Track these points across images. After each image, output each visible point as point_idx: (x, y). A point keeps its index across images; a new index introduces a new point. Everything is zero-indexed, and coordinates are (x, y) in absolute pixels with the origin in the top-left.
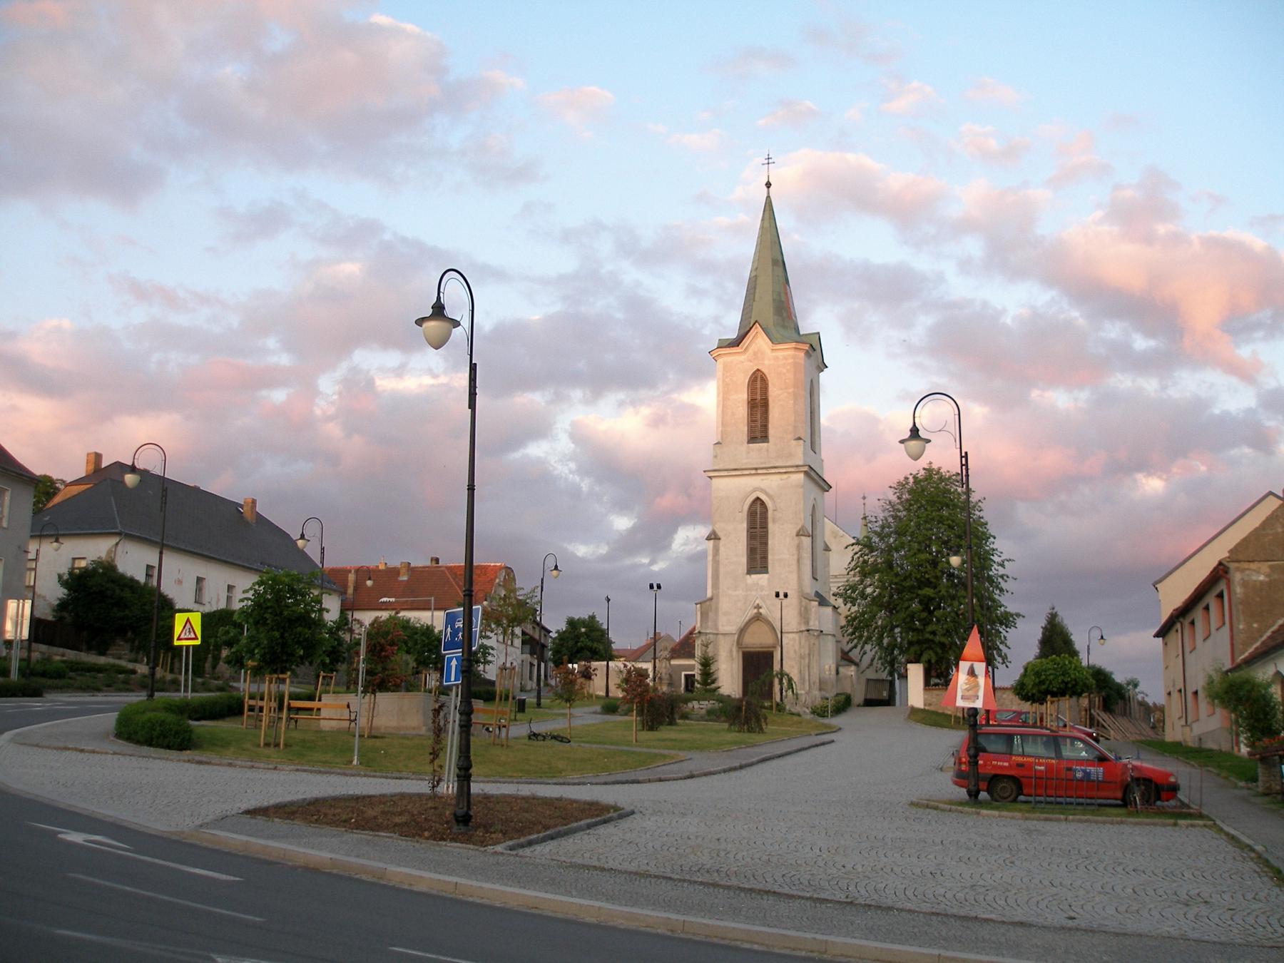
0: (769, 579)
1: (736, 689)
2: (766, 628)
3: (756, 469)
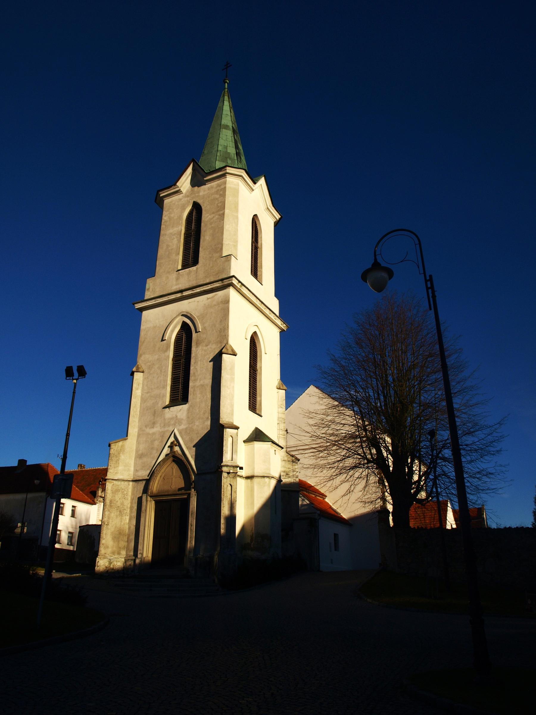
0: (188, 410)
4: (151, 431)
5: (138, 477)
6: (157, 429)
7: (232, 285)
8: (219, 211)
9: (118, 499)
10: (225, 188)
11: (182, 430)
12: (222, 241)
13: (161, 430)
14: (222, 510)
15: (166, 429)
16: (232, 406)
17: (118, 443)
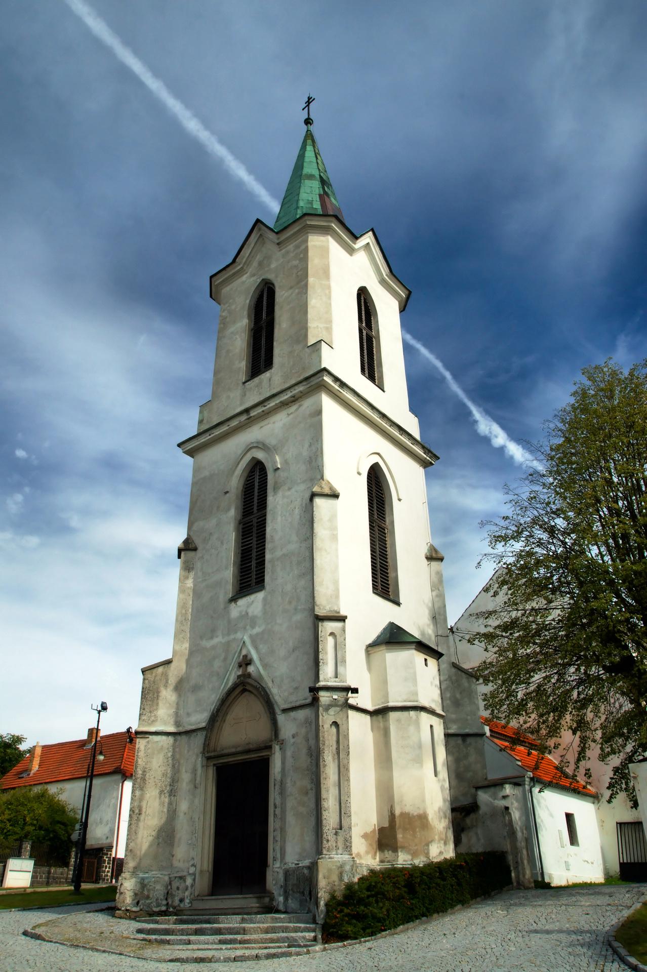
0: (265, 599)
1: (197, 861)
2: (258, 706)
3: (247, 411)
4: (207, 644)
5: (191, 725)
6: (219, 640)
7: (323, 387)
8: (298, 283)
9: (157, 767)
10: (307, 247)
11: (257, 634)
12: (307, 323)
13: (223, 641)
14: (321, 773)
15: (232, 637)
16: (336, 583)
17: (156, 669)
